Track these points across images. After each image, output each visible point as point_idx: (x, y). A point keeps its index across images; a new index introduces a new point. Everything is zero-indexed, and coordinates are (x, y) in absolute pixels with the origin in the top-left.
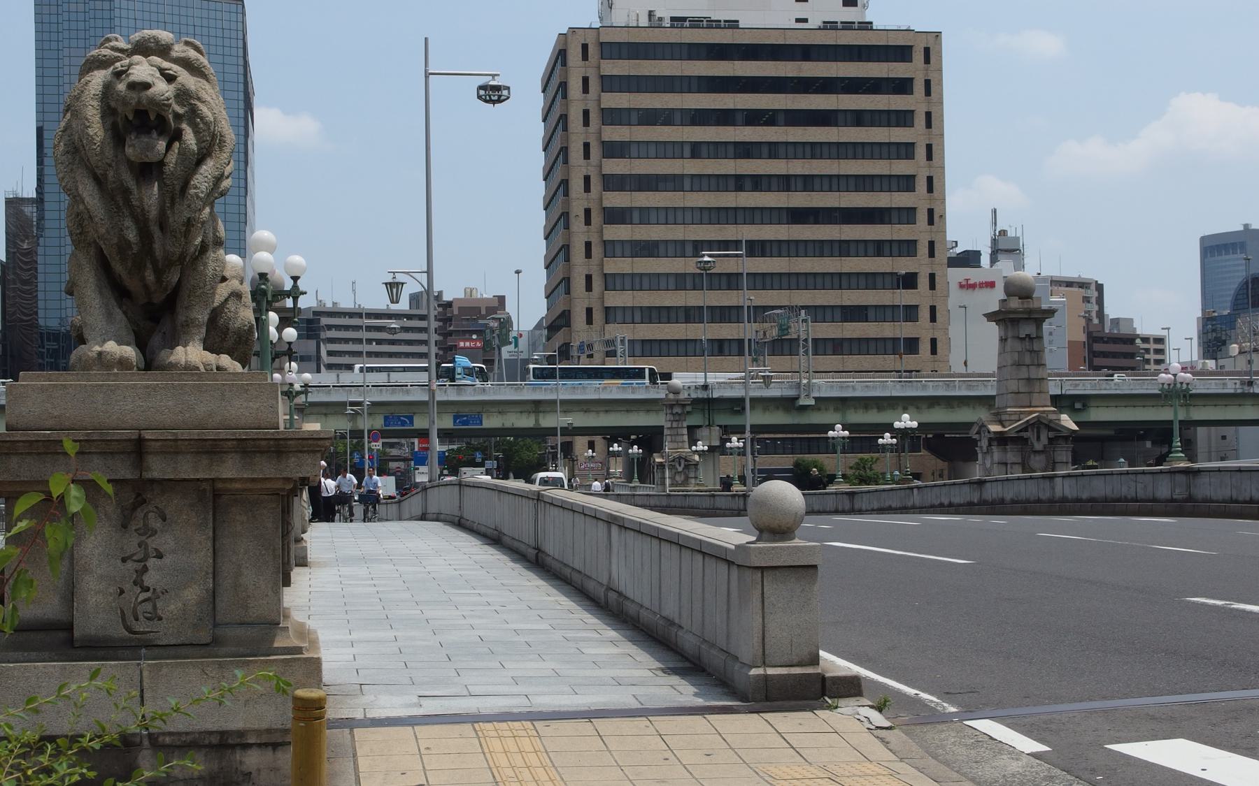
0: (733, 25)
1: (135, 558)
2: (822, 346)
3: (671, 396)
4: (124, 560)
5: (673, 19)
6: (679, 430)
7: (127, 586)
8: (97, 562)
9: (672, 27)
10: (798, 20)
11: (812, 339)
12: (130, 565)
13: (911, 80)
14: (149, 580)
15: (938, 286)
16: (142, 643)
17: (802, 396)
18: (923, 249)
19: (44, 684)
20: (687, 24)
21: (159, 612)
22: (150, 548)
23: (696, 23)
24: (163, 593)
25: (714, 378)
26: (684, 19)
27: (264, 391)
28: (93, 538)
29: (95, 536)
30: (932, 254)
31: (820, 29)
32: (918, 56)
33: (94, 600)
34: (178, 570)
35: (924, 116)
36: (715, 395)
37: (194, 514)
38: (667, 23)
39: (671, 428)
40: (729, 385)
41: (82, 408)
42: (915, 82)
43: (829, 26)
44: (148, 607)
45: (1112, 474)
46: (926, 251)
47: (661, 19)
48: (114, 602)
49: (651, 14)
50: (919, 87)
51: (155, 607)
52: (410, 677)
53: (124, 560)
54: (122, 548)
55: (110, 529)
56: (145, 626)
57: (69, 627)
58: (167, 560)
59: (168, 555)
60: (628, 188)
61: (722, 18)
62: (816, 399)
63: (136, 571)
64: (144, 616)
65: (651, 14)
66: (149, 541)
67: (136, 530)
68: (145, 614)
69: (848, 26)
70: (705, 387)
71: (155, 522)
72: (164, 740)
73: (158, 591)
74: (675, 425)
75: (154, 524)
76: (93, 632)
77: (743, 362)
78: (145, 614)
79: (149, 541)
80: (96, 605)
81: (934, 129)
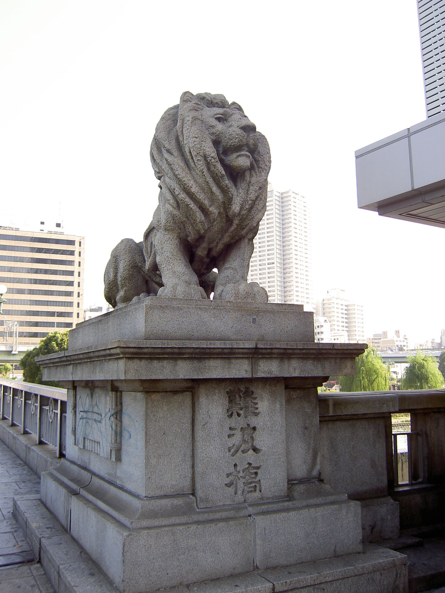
0: (17, 230)
2: (22, 335)
10: (41, 230)
11: (19, 332)
15: (80, 317)
17: (14, 350)
32: (77, 244)
35: (78, 263)
42: (75, 252)
43: (50, 232)
46: (77, 305)
52: (40, 500)
60: (58, 274)
61: (14, 227)
62: (19, 352)
69: (56, 233)
77: (12, 339)
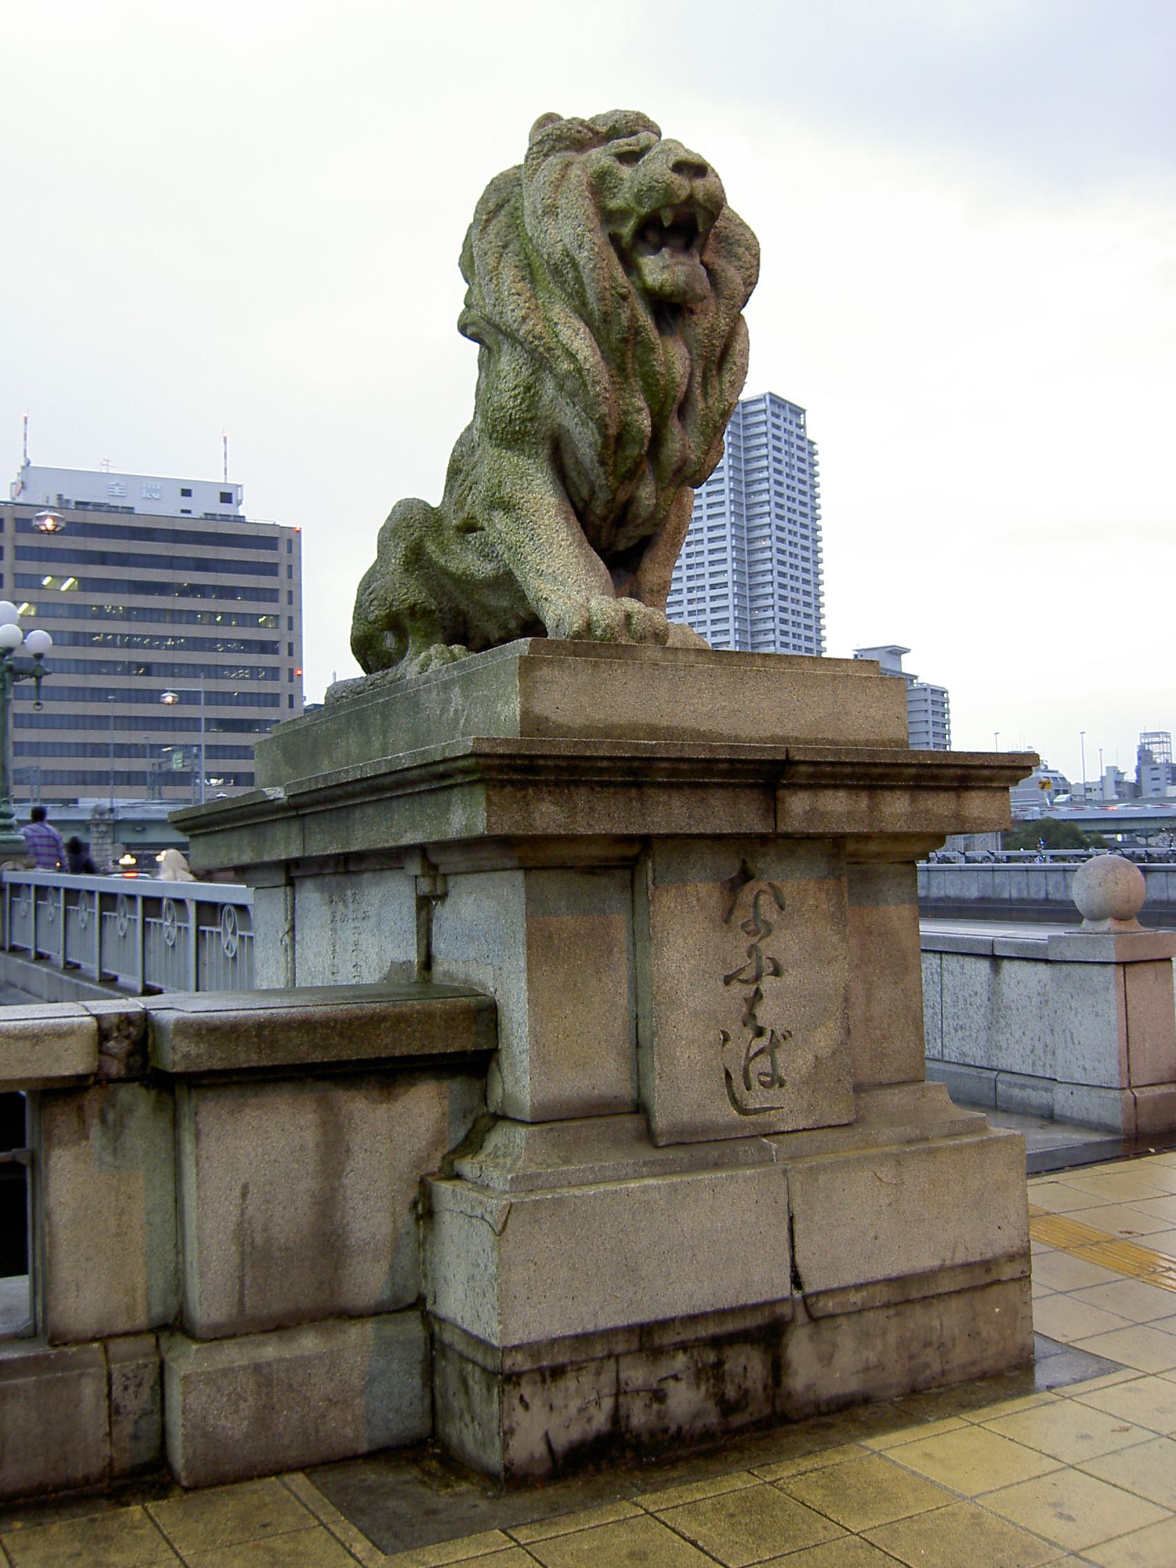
0: (129, 510)
1: (743, 977)
3: (97, 817)
4: (727, 980)
5: (77, 503)
6: (105, 847)
7: (734, 1028)
8: (689, 987)
9: (76, 509)
10: (183, 511)
12: (736, 987)
13: (276, 565)
14: (766, 1014)
16: (759, 1129)
18: (284, 702)
19: (642, 1225)
20: (90, 507)
21: (782, 1072)
22: (764, 957)
23: (98, 507)
24: (785, 1038)
25: (119, 802)
26: (87, 504)
27: (887, 690)
28: (680, 941)
29: (685, 939)
30: (291, 705)
31: (201, 519)
32: (283, 547)
33: (686, 1056)
34: (805, 997)
36: (120, 818)
37: (824, 896)
38: (72, 506)
39: (96, 844)
40: (132, 807)
41: (637, 706)
43: (210, 517)
44: (763, 1064)
45: (993, 871)
47: (68, 501)
48: (716, 1059)
49: (60, 497)
50: (283, 571)
51: (773, 1063)
53: (727, 980)
54: (724, 961)
55: (705, 925)
56: (762, 1099)
57: (640, 1108)
58: (790, 978)
59: (790, 969)
63: (746, 1000)
64: (760, 1081)
65: (60, 497)
66: (762, 945)
67: (743, 926)
68: (763, 1078)
69: (225, 518)
70: (112, 810)
71: (768, 911)
72: (826, 1305)
73: (778, 1034)
74: (100, 841)
75: (768, 915)
76: (686, 1117)
78: (763, 1078)
79: (762, 945)
80: (690, 1066)
81: (294, 606)
